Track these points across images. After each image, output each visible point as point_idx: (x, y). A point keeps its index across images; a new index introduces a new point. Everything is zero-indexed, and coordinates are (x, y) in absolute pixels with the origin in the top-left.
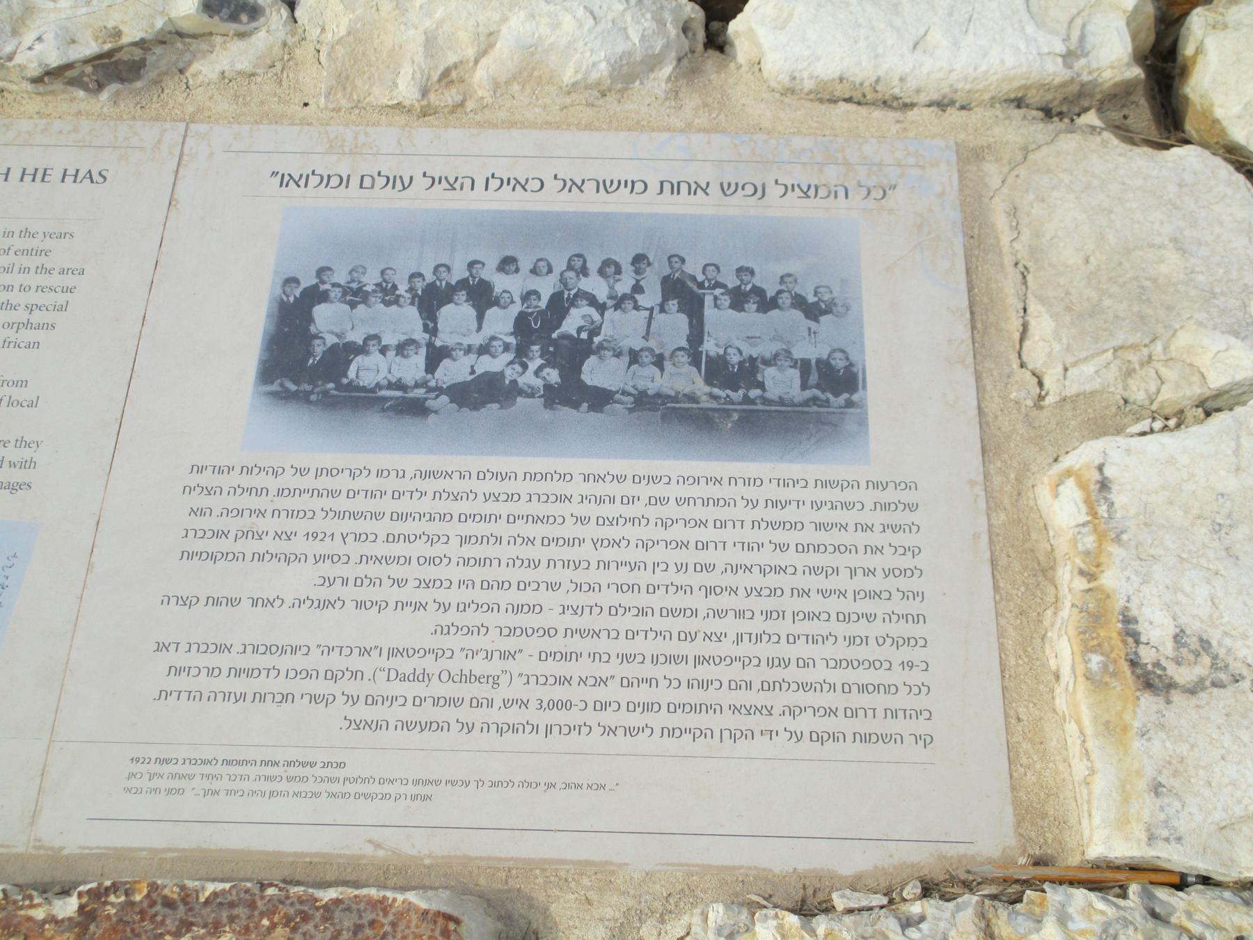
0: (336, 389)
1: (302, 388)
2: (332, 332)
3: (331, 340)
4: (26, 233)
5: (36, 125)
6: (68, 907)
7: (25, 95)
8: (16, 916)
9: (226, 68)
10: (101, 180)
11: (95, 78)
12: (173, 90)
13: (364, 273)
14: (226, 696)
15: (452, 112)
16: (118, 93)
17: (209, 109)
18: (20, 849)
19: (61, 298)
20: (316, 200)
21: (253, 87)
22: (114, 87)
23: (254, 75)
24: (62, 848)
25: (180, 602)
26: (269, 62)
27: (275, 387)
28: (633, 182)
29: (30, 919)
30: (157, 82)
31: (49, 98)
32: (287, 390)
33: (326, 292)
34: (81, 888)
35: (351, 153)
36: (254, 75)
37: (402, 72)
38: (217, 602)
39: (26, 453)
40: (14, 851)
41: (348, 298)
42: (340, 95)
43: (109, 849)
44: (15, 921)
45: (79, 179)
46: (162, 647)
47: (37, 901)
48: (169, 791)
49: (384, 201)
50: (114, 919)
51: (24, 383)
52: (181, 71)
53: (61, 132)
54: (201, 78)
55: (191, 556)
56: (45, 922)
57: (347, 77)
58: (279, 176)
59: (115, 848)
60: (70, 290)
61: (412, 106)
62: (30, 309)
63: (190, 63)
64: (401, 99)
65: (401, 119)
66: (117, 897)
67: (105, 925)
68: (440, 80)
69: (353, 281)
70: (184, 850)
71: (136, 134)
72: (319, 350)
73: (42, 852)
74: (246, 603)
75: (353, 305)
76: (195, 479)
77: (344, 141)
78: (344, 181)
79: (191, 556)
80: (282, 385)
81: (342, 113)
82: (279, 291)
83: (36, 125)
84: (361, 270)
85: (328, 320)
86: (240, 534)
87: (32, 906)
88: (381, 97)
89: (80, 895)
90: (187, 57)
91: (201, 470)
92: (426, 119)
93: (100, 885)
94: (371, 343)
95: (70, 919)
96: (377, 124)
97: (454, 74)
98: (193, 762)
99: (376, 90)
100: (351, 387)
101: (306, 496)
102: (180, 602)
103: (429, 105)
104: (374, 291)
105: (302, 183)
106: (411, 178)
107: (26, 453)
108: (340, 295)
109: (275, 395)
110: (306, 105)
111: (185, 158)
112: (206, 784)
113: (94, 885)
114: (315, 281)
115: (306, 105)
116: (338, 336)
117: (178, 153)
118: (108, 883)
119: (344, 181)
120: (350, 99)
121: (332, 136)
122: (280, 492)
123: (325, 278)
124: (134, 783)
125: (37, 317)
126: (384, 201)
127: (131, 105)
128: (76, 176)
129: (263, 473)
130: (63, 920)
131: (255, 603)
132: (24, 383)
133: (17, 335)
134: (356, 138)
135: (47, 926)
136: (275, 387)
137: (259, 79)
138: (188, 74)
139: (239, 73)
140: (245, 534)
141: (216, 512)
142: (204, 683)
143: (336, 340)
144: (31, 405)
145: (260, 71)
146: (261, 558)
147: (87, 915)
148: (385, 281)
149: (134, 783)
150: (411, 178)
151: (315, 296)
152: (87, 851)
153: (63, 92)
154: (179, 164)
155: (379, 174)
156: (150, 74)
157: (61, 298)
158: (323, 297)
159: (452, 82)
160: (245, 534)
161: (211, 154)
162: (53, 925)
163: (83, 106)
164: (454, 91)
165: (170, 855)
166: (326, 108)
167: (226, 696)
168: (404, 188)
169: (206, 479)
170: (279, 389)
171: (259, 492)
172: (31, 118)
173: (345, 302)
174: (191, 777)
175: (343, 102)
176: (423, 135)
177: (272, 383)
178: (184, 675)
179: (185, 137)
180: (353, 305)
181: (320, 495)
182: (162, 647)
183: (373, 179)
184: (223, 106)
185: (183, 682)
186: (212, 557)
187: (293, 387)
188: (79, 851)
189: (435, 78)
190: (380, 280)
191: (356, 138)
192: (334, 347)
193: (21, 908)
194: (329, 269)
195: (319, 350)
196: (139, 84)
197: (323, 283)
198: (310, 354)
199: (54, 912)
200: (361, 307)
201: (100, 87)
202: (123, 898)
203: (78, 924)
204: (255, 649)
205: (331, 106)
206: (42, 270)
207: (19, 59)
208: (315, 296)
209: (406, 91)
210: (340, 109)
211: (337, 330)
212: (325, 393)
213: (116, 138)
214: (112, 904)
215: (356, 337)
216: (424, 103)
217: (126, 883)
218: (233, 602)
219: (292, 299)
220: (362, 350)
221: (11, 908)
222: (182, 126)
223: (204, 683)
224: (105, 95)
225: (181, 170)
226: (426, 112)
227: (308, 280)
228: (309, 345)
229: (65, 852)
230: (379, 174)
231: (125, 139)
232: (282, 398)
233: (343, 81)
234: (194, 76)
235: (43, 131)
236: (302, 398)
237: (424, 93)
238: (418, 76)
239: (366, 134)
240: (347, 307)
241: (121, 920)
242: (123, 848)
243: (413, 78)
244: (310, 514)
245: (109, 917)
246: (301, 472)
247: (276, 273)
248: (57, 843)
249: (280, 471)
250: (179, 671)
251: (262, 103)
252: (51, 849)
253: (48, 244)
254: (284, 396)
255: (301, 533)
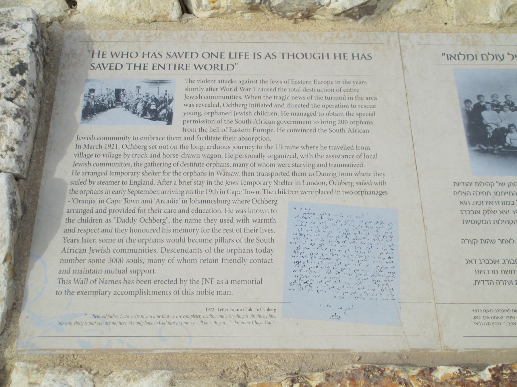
0: (503, 148)
1: (489, 148)
2: (493, 123)
3: (494, 127)
4: (345, 82)
5: (333, 34)
6: (486, 375)
7: (326, 21)
8: (466, 380)
9: (409, 8)
10: (160, 57)
11: (358, 13)
12: (385, 17)
13: (498, 97)
14: (504, 282)
15: (511, 26)
16: (366, 20)
17: (405, 26)
18: (439, 351)
19: (371, 110)
20: (478, 65)
21: (420, 16)
22: (365, 17)
23: (419, 11)
24: (457, 350)
25: (470, 242)
26: (425, 5)
27: (477, 148)
28: (468, 55)
29: (472, 381)
30: (379, 15)
31: (336, 22)
32: (483, 149)
33: (484, 106)
34: (489, 367)
35: (473, 45)
36: (419, 11)
37: (491, 9)
38: (485, 242)
39: (380, 179)
40: (436, 351)
41: (495, 108)
42: (462, 19)
43: (478, 349)
44: (466, 383)
45: (150, 56)
46: (469, 262)
47: (473, 374)
48: (494, 324)
49: (494, 65)
50: (508, 380)
51: (368, 148)
52: (388, 10)
53: (344, 37)
54: (397, 13)
55: (467, 222)
56: (479, 383)
57: (464, 12)
58: (446, 55)
59: (480, 349)
60: (374, 107)
61: (496, 24)
62: (359, 115)
63: (391, 6)
64: (491, 21)
65: (490, 30)
66: (507, 371)
67: (506, 383)
68: (507, 12)
69: (494, 101)
70: (509, 349)
71: (377, 38)
72: (490, 131)
73: (449, 351)
74: (498, 242)
75: (498, 112)
76: (457, 189)
77: (468, 39)
78: (475, 57)
79: (467, 222)
80: (480, 147)
81: (463, 27)
82: (464, 106)
83: (333, 34)
84: (496, 96)
85: (488, 116)
86: (485, 212)
87: (471, 376)
88: (480, 19)
89: (490, 370)
90: (390, 4)
91: (458, 184)
92: (500, 29)
93: (497, 366)
94: (512, 128)
95: (490, 381)
96: (480, 32)
97: (511, 10)
98: (501, 311)
99: (478, 17)
100: (509, 147)
101: (507, 195)
102: (470, 242)
103: (502, 24)
104: (505, 105)
105: (457, 58)
106: (503, 55)
107: (380, 179)
108: (490, 107)
109: (478, 151)
110: (446, 24)
111: (402, 48)
112: (509, 321)
113: (494, 366)
114: (477, 101)
115: (446, 24)
116: (497, 125)
117: (398, 46)
118: (500, 365)
119: (475, 57)
120: (466, 21)
121: (462, 37)
122: (496, 193)
123: (481, 100)
124: (478, 321)
125: (363, 119)
126: (494, 65)
127: (370, 25)
128: (358, 56)
129: (485, 186)
130: (487, 382)
131: (502, 241)
132: (368, 148)
133: (358, 127)
134: (473, 38)
135: (481, 384)
136: (477, 148)
137: (422, 13)
138: (391, 11)
139: (414, 10)
140: (487, 212)
141: (471, 203)
142: (491, 277)
143: (496, 127)
144: (374, 158)
145: (422, 9)
146: (498, 222)
147: (496, 379)
148: (507, 100)
149: (478, 321)
150: (503, 55)
151: (479, 108)
152: (468, 351)
153: (343, 20)
154: (401, 51)
155: (488, 53)
156: (377, 11)
157: (371, 110)
158: (484, 108)
159: (510, 13)
160: (487, 212)
161: (413, 46)
162: (483, 384)
163: (351, 26)
164: (512, 17)
165: (504, 351)
166: (457, 25)
167: (504, 282)
168: (502, 60)
169: (461, 188)
170: (479, 148)
171: (487, 193)
172: (329, 31)
173: (494, 110)
174: (502, 317)
175: (464, 22)
176: (502, 36)
177: (475, 146)
178: (483, 273)
179: (399, 39)
180: (498, 112)
181: (513, 194)
182: (469, 262)
183: (487, 56)
184: (410, 25)
185: (482, 277)
186: (476, 222)
187: (485, 148)
188: (464, 351)
189: (505, 11)
190: (505, 100)
191: (473, 38)
192: (496, 130)
193: (467, 377)
194: (482, 96)
195: (490, 131)
196: (373, 16)
197: (482, 102)
198: (487, 133)
199: (482, 378)
200: (501, 112)
201: (360, 17)
202: (509, 371)
203: (494, 383)
204: (509, 262)
205: (459, 24)
206: (357, 98)
207: (332, 6)
208: (479, 108)
209: (493, 16)
210: (462, 26)
211: (495, 122)
212: (500, 150)
213: (370, 40)
214: (506, 374)
215: (504, 125)
216: (501, 22)
217: (509, 365)
218: (493, 242)
219: (471, 109)
220: (508, 131)
221: (462, 377)
222: (396, 34)
223: (491, 277)
224: (361, 21)
225: (402, 53)
226: (501, 26)
227: (475, 101)
228: (485, 129)
229: (459, 351)
230: (488, 53)
231: (374, 40)
232: (482, 153)
233: (462, 13)
234: (394, 12)
235: (337, 37)
236: (490, 152)
237: (501, 18)
238: (499, 10)
239: (476, 36)
240: (495, 112)
241: (511, 381)
242: (483, 349)
243: (497, 12)
244: (512, 203)
245: (506, 379)
246: (502, 184)
247: (460, 98)
248: (454, 347)
249: (493, 184)
250: (480, 272)
251: (426, 23)
252: (453, 350)
253: (357, 87)
254: (482, 152)
255: (511, 211)
